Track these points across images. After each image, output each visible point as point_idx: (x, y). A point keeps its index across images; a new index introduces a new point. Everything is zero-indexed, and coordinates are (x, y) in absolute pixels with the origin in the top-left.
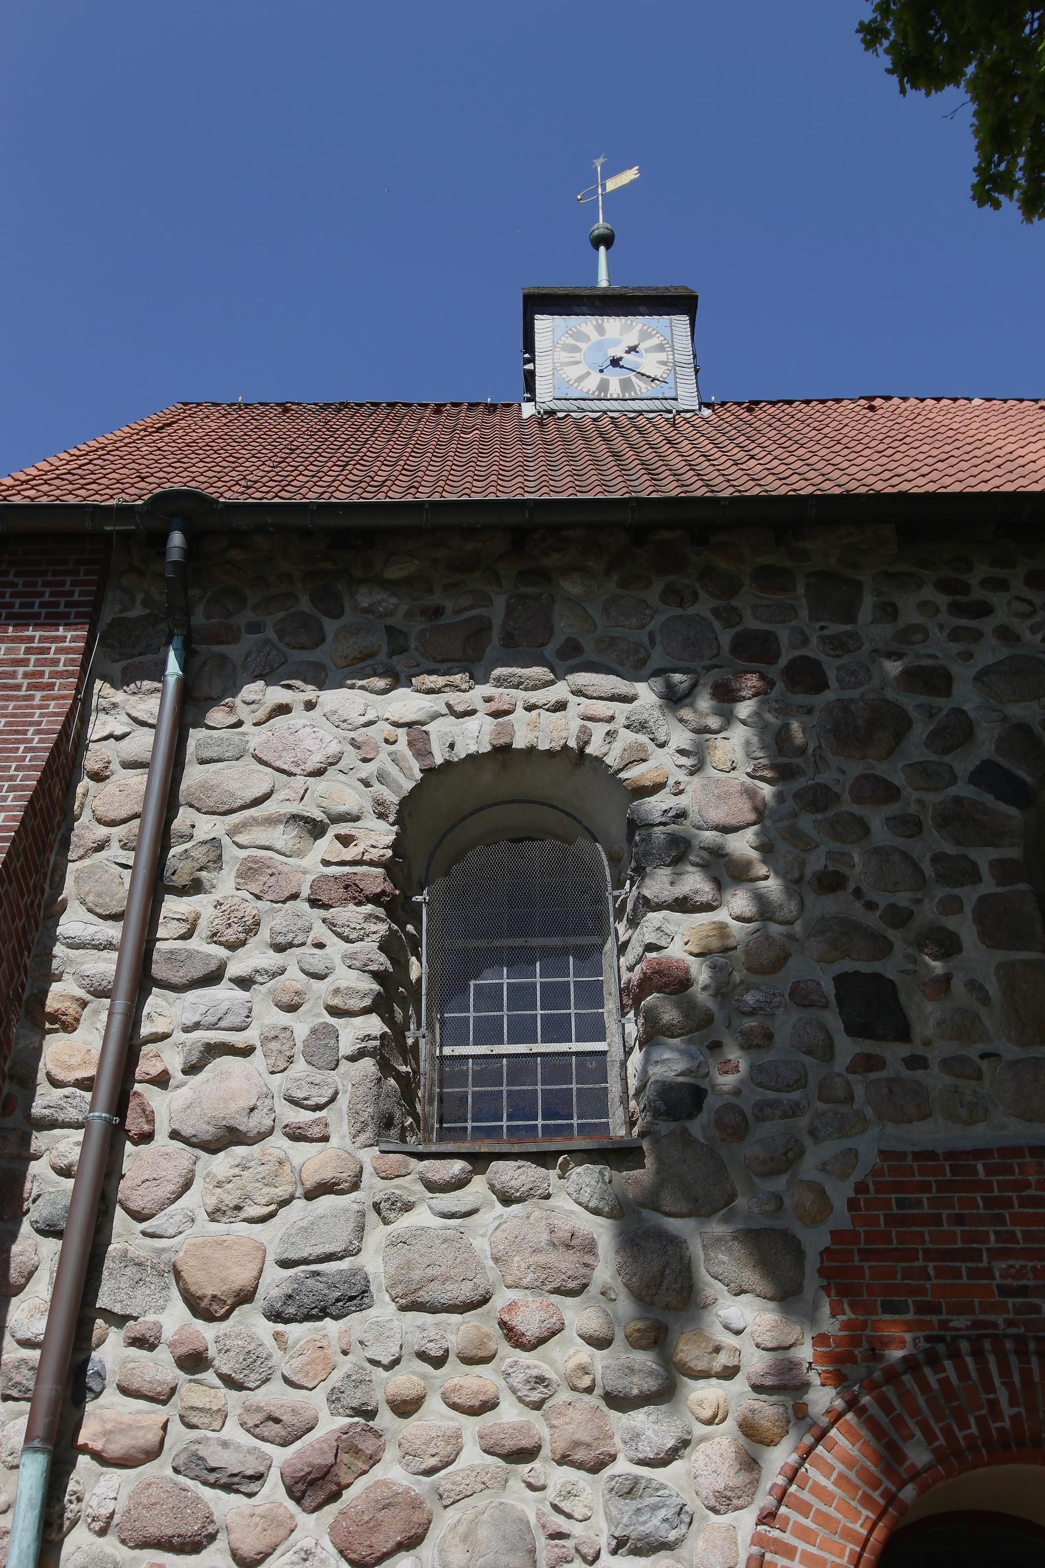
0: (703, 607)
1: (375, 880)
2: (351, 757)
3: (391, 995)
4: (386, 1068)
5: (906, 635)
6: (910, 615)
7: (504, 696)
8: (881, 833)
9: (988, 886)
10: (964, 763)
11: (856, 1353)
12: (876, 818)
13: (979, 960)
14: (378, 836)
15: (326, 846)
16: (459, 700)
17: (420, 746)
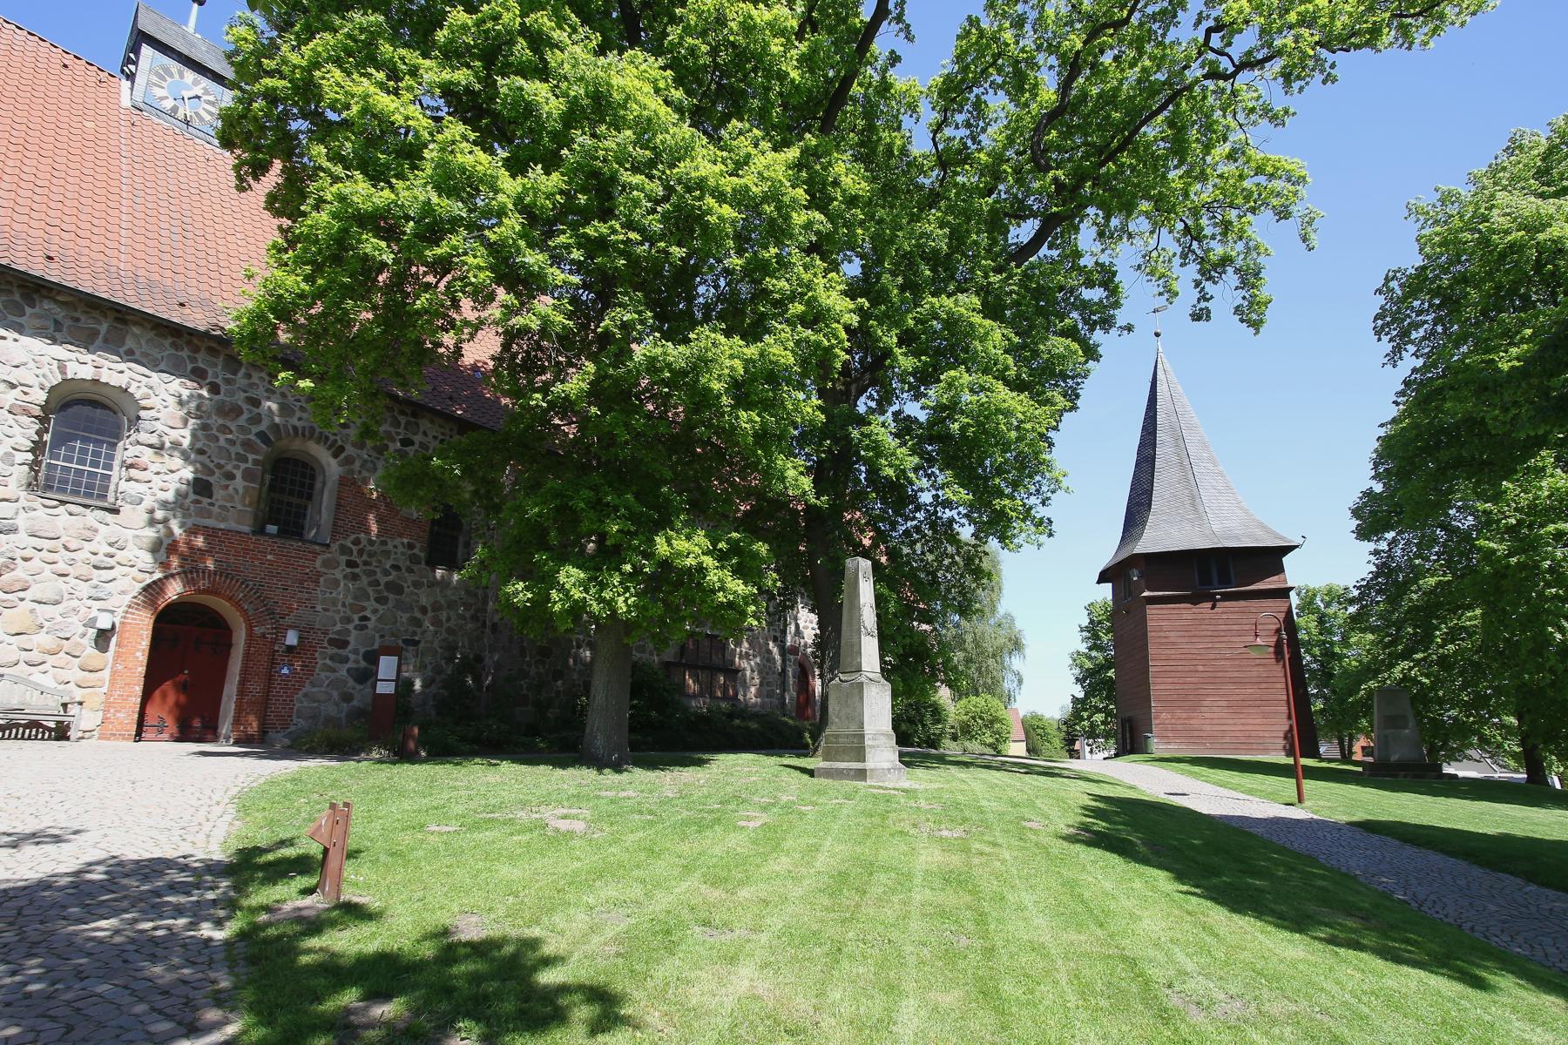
0: (185, 353)
1: (37, 411)
2: (32, 365)
3: (37, 448)
4: (31, 469)
5: (252, 385)
6: (255, 379)
7: (100, 361)
8: (222, 442)
9: (249, 465)
10: (255, 429)
11: (895, 340)
12: (222, 438)
13: (239, 482)
14: (42, 397)
15: (17, 392)
16: (83, 358)
17: (62, 369)
